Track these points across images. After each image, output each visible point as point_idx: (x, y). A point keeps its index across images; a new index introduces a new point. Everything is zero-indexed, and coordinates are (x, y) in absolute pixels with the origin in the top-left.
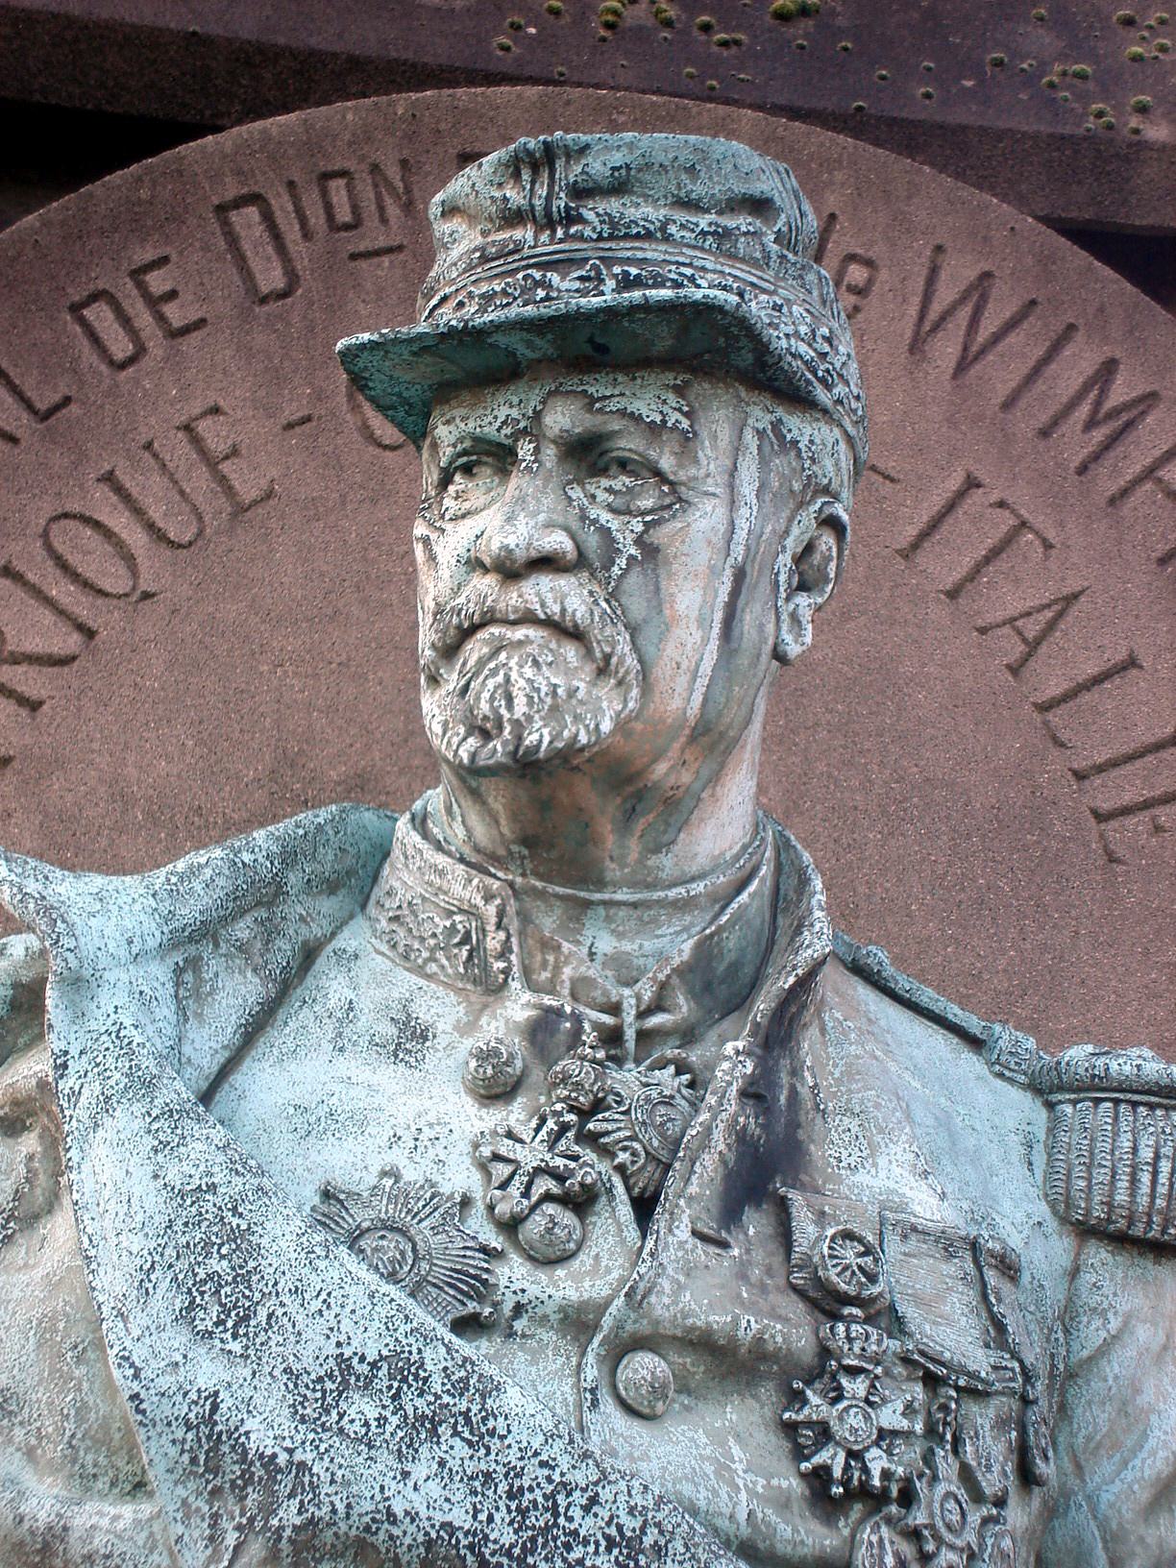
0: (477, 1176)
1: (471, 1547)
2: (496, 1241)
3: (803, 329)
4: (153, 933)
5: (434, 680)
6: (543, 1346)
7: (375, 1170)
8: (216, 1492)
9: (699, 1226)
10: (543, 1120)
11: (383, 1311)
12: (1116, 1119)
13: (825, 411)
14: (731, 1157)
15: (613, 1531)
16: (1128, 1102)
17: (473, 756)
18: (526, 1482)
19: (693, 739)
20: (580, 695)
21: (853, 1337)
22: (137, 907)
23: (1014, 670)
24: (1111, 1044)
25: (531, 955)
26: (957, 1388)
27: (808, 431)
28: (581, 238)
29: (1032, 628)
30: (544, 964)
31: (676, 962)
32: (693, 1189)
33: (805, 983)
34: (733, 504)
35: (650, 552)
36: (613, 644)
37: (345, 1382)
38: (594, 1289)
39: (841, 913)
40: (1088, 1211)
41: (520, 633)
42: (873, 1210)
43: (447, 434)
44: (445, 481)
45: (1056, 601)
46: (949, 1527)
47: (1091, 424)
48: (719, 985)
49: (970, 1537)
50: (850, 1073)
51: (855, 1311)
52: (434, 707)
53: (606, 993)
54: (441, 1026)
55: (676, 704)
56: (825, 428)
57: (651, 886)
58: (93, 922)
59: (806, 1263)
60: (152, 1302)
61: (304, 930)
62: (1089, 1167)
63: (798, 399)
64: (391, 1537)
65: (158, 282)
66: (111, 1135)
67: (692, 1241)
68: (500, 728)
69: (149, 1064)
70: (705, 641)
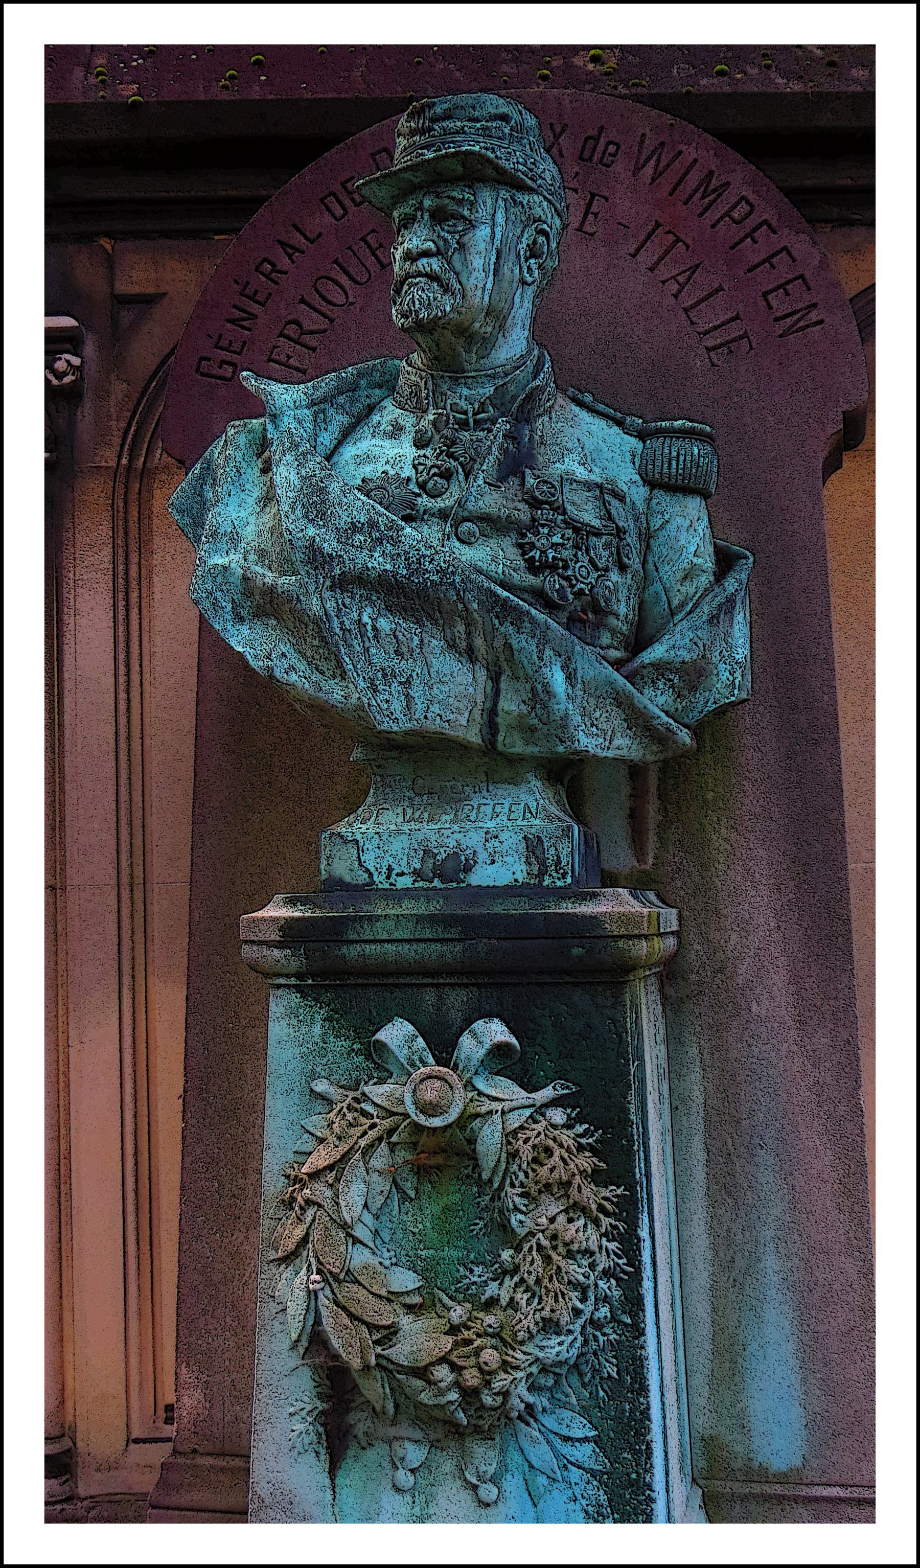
1: (393, 576)
2: (417, 491)
8: (316, 568)
9: (487, 480)
10: (436, 450)
12: (664, 443)
23: (676, 296)
26: (586, 530)
27: (527, 198)
28: (433, 136)
29: (681, 279)
35: (462, 246)
46: (581, 576)
47: (703, 197)
54: (407, 425)
56: (535, 197)
61: (368, 400)
63: (521, 187)
66: (285, 462)
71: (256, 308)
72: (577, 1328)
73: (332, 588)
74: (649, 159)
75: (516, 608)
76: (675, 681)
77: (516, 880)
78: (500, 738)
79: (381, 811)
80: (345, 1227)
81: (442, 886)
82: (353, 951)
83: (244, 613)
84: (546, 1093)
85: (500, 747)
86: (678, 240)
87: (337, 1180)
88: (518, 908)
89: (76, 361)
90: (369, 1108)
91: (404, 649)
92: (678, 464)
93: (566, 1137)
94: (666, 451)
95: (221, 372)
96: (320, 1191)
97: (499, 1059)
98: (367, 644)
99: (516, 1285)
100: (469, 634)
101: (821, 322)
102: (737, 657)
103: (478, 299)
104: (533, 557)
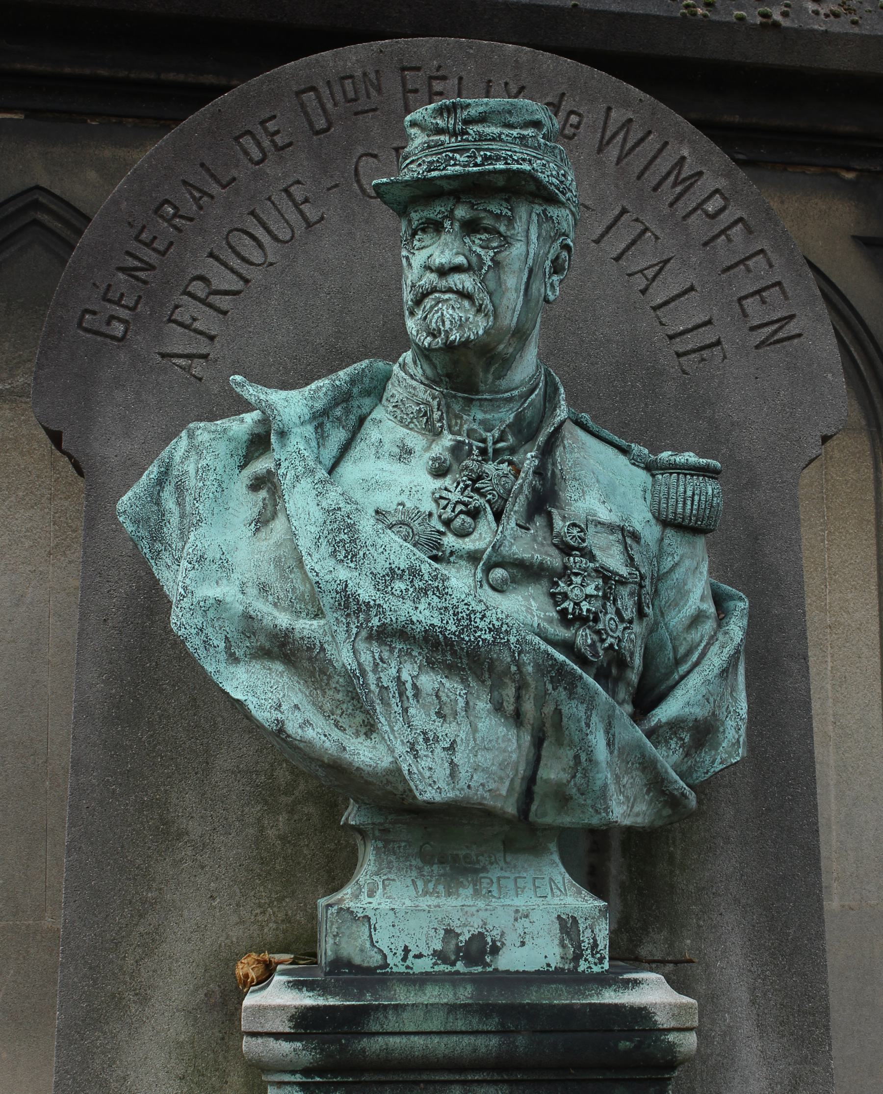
0: (434, 505)
2: (442, 529)
3: (554, 173)
4: (306, 413)
5: (412, 314)
6: (461, 566)
7: (395, 503)
8: (348, 615)
10: (458, 484)
11: (406, 552)
12: (678, 480)
13: (563, 204)
14: (530, 496)
15: (491, 626)
16: (689, 474)
17: (430, 344)
18: (460, 610)
19: (513, 335)
20: (471, 320)
21: (576, 561)
22: (300, 404)
24: (679, 450)
25: (451, 420)
26: (615, 581)
29: (650, 273)
30: (456, 424)
31: (508, 422)
32: (516, 508)
34: (528, 244)
35: (497, 264)
36: (483, 300)
37: (393, 577)
38: (480, 545)
39: (572, 400)
40: (667, 515)
41: (447, 296)
42: (583, 516)
43: (415, 217)
44: (414, 234)
45: (660, 262)
46: (611, 630)
47: (675, 184)
48: (524, 431)
49: (618, 634)
50: (575, 464)
51: (577, 553)
52: (411, 325)
53: (481, 435)
55: (507, 322)
56: (563, 210)
57: (497, 393)
58: (286, 410)
59: (558, 535)
60: (320, 550)
61: (359, 411)
62: (667, 499)
64: (413, 629)
65: (271, 126)
66: (300, 490)
67: (516, 528)
68: (440, 333)
69: (312, 464)
70: (518, 297)
75: (572, 673)
76: (686, 740)
77: (548, 965)
78: (534, 807)
79: (386, 882)
81: (466, 970)
82: (374, 1046)
83: (239, 653)
85: (532, 817)
88: (563, 997)
91: (447, 711)
92: (692, 504)
94: (681, 489)
98: (406, 705)
100: (518, 698)
102: (741, 712)
103: (509, 320)
104: (566, 609)
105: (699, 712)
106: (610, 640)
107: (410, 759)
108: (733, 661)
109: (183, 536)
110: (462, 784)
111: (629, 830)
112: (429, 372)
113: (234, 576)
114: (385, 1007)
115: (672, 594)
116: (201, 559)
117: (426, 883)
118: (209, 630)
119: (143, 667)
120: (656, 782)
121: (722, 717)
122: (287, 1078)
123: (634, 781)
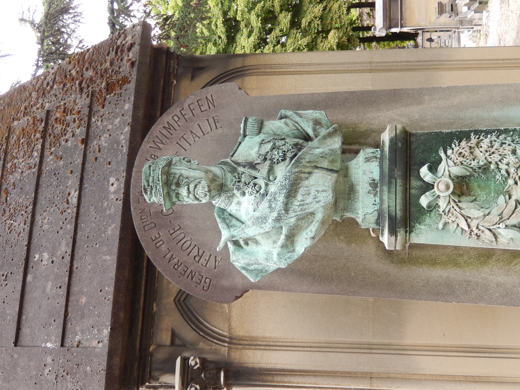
4: (227, 230)
5: (201, 201)
29: (194, 136)
33: (233, 162)
35: (187, 178)
44: (180, 200)
47: (170, 129)
48: (233, 170)
49: (288, 145)
52: (204, 201)
71: (189, 271)
72: (514, 145)
73: (287, 213)
74: (158, 146)
75: (298, 159)
78: (335, 169)
80: (485, 216)
82: (399, 213)
83: (292, 249)
84: (443, 155)
86: (183, 137)
87: (470, 218)
88: (386, 163)
89: (192, 358)
90: (447, 210)
91: (308, 193)
93: (456, 149)
95: (208, 283)
96: (474, 224)
97: (433, 169)
99: (502, 163)
100: (304, 173)
101: (212, 96)
103: (203, 174)
105: (311, 124)
106: (290, 148)
107: (321, 203)
108: (297, 114)
109: (261, 264)
110: (328, 189)
111: (343, 143)
112: (217, 196)
113: (271, 250)
114: (388, 210)
115: (279, 131)
116: (267, 259)
117: (356, 199)
118: (286, 257)
119: (305, 273)
120: (330, 135)
121: (313, 117)
122: (408, 237)
123: (329, 141)
